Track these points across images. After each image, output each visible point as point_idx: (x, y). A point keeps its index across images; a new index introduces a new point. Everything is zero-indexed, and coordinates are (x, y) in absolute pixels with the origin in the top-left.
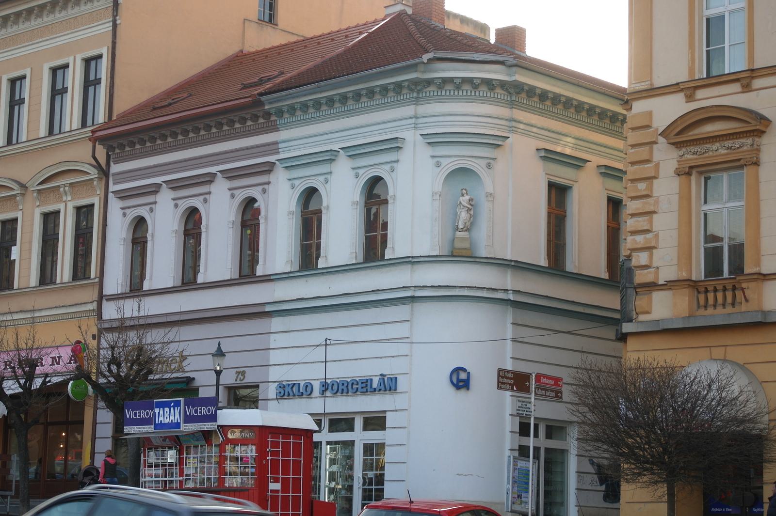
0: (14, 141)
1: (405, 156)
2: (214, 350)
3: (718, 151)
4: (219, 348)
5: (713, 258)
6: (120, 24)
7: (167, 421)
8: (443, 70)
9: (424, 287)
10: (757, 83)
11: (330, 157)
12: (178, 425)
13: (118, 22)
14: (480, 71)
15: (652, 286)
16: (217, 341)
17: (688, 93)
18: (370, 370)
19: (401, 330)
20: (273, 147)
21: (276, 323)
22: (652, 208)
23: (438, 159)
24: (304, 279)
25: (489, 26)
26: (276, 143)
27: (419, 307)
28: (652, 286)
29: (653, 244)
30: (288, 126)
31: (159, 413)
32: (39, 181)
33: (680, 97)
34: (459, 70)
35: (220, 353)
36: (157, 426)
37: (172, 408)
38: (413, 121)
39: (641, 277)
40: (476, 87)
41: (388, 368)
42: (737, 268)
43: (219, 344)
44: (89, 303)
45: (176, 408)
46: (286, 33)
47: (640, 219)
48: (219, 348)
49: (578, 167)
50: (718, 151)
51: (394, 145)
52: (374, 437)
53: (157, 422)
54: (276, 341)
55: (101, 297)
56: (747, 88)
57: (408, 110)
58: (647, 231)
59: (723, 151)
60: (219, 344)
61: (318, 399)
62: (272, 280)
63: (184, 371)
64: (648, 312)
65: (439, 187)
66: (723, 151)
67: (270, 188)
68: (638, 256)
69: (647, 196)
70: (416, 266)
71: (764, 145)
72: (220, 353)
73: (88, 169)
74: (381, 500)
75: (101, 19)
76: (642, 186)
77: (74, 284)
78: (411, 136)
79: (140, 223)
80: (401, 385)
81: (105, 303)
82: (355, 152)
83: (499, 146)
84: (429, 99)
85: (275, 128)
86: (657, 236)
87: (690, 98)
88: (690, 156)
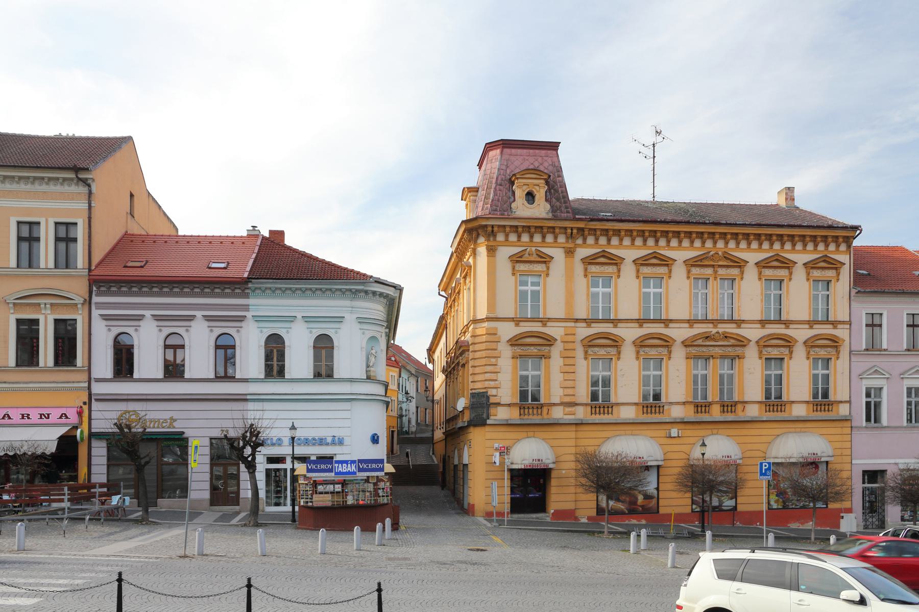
2: (290, 425)
3: (533, 350)
4: (293, 425)
5: (523, 395)
6: (94, 206)
7: (345, 471)
8: (374, 287)
9: (360, 394)
11: (292, 319)
12: (354, 473)
13: (92, 205)
14: (387, 290)
15: (498, 404)
16: (292, 421)
17: (517, 323)
18: (327, 434)
19: (346, 414)
20: (246, 308)
22: (499, 371)
23: (363, 331)
24: (273, 383)
26: (248, 305)
27: (354, 403)
28: (498, 404)
29: (499, 386)
30: (256, 297)
31: (338, 467)
32: (16, 298)
33: (512, 324)
34: (380, 288)
35: (293, 428)
36: (336, 474)
37: (349, 465)
38: (350, 309)
39: (492, 400)
40: (344, 293)
41: (338, 433)
42: (535, 398)
43: (293, 423)
44: (82, 382)
45: (352, 464)
47: (492, 375)
48: (293, 425)
49: (241, 321)
51: (340, 320)
53: (336, 471)
57: (347, 303)
58: (496, 380)
59: (536, 351)
60: (293, 423)
61: (287, 447)
62: (248, 382)
63: (174, 427)
64: (496, 415)
65: (364, 344)
66: (536, 351)
68: (491, 391)
69: (496, 365)
70: (353, 383)
72: (293, 428)
73: (71, 296)
74: (55, 483)
75: (73, 200)
76: (493, 360)
77: (54, 369)
78: (350, 318)
80: (347, 441)
83: (342, 322)
85: (247, 296)
86: (500, 383)
87: (517, 325)
88: (518, 350)
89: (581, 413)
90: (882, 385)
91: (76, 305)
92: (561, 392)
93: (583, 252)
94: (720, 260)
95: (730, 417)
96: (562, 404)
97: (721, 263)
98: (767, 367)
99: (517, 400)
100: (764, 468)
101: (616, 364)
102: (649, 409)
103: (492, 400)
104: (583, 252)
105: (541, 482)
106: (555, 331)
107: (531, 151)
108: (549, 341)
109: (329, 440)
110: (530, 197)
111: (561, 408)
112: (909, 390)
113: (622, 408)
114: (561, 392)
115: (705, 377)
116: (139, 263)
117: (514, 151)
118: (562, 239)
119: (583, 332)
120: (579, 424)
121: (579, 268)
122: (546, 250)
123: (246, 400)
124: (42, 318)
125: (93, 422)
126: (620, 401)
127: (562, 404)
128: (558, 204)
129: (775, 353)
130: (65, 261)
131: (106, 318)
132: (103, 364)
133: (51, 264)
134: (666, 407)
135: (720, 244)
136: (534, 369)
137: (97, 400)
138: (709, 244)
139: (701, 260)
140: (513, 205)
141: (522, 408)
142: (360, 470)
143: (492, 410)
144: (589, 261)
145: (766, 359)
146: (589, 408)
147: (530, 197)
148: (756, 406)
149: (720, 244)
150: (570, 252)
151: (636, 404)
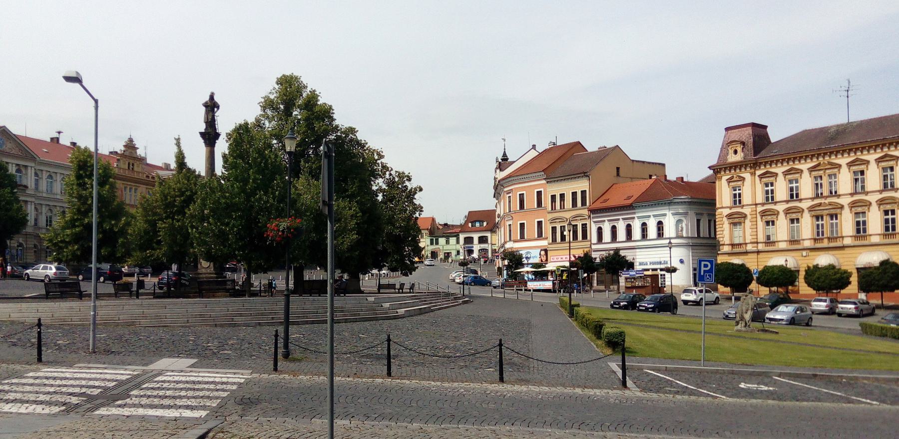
0: (554, 209)
1: (667, 217)
10: (744, 207)
11: (649, 217)
15: (724, 245)
21: (637, 250)
25: (781, 264)
28: (724, 245)
39: (721, 243)
46: (553, 165)
50: (736, 220)
52: (740, 192)
54: (637, 254)
55: (591, 243)
56: (742, 208)
64: (723, 249)
67: (634, 222)
71: (870, 235)
76: (721, 225)
79: (644, 224)
81: (592, 245)
82: (655, 216)
84: (672, 205)
85: (634, 209)
87: (730, 209)
88: (731, 221)
89: (761, 247)
90: (450, 250)
91: (586, 219)
92: (750, 237)
93: (759, 172)
94: (826, 166)
95: (832, 245)
96: (751, 243)
97: (826, 167)
98: (856, 217)
99: (855, 234)
100: (703, 269)
101: (868, 213)
102: (833, 240)
103: (721, 243)
104: (759, 172)
105: (8, 270)
106: (747, 211)
107: (740, 129)
108: (745, 216)
109: (663, 262)
110: (736, 152)
111: (751, 245)
112: (445, 253)
113: (780, 243)
114: (750, 237)
115: (822, 225)
116: (756, 181)
117: (733, 131)
118: (748, 169)
119: (760, 209)
120: (758, 252)
121: (757, 179)
122: (742, 175)
123: (636, 248)
124: (557, 226)
125: (669, 256)
126: (778, 240)
127: (751, 243)
128: (748, 152)
129: (860, 210)
130: (584, 203)
131: (595, 222)
132: (594, 239)
133: (559, 208)
134: (801, 242)
135: (827, 158)
136: (863, 217)
137: (593, 251)
138: (821, 159)
139: (855, 162)
140: (728, 157)
141: (815, 240)
142: (637, 274)
143: (721, 247)
144: (761, 176)
145: (856, 213)
146: (882, 236)
147: (736, 152)
148: (850, 239)
149: (827, 158)
150: (753, 174)
151: (879, 235)
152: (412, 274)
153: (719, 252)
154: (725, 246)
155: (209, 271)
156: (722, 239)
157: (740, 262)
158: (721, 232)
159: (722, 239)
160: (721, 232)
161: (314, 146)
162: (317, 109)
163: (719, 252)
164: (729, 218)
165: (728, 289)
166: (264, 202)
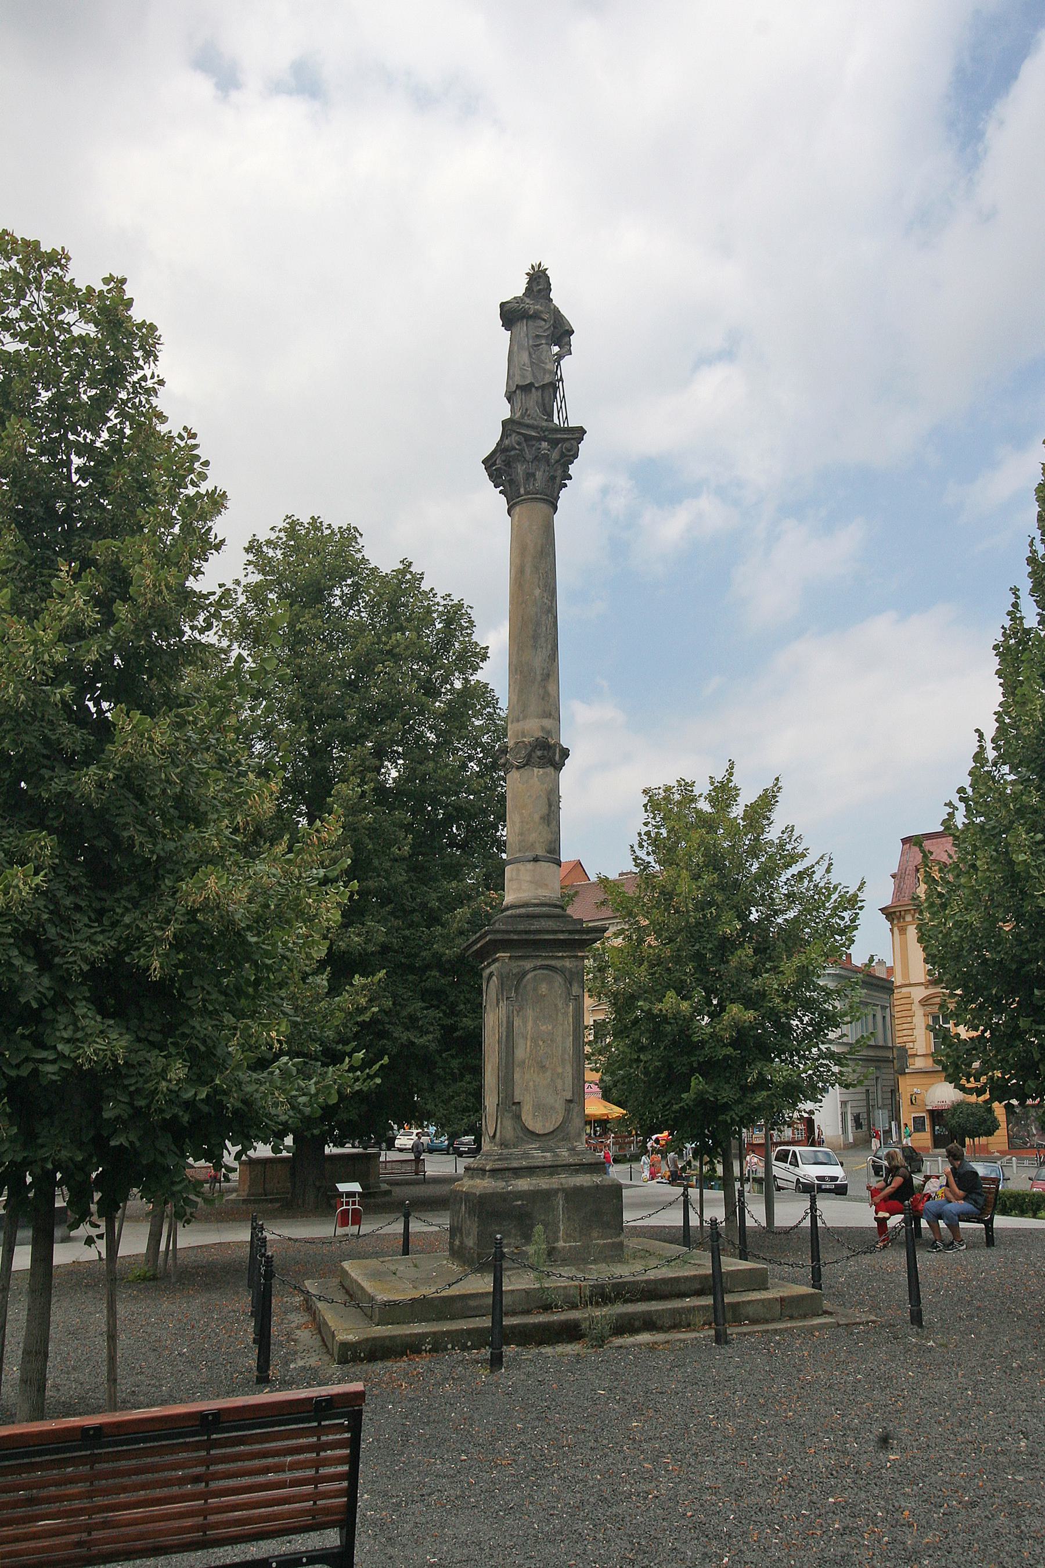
15: (916, 1055)
28: (916, 1055)
39: (910, 1052)
103: (910, 1052)
143: (910, 1061)
152: (996, 655)
153: (907, 1071)
154: (917, 1059)
155: (564, 1155)
156: (911, 1045)
157: (118, 1143)
158: (909, 1032)
159: (911, 1045)
160: (909, 1032)
161: (109, 507)
162: (448, 1212)
163: (907, 1071)
164: (924, 1005)
165: (666, 1133)
166: (47, 799)
